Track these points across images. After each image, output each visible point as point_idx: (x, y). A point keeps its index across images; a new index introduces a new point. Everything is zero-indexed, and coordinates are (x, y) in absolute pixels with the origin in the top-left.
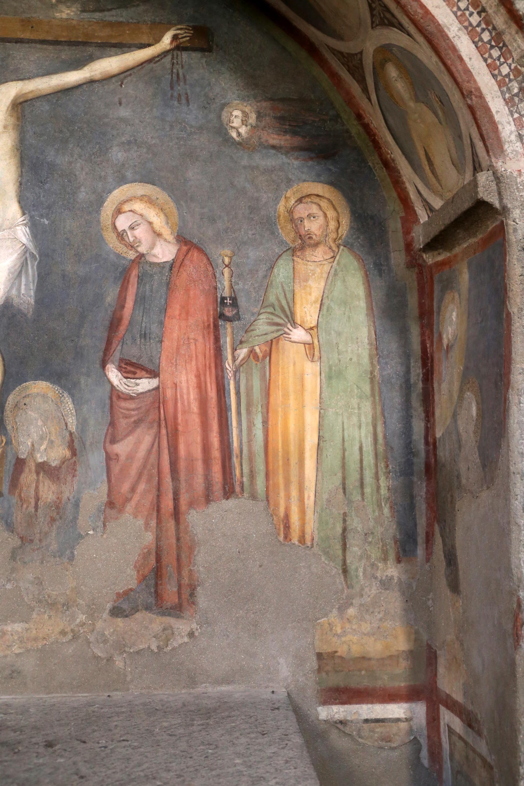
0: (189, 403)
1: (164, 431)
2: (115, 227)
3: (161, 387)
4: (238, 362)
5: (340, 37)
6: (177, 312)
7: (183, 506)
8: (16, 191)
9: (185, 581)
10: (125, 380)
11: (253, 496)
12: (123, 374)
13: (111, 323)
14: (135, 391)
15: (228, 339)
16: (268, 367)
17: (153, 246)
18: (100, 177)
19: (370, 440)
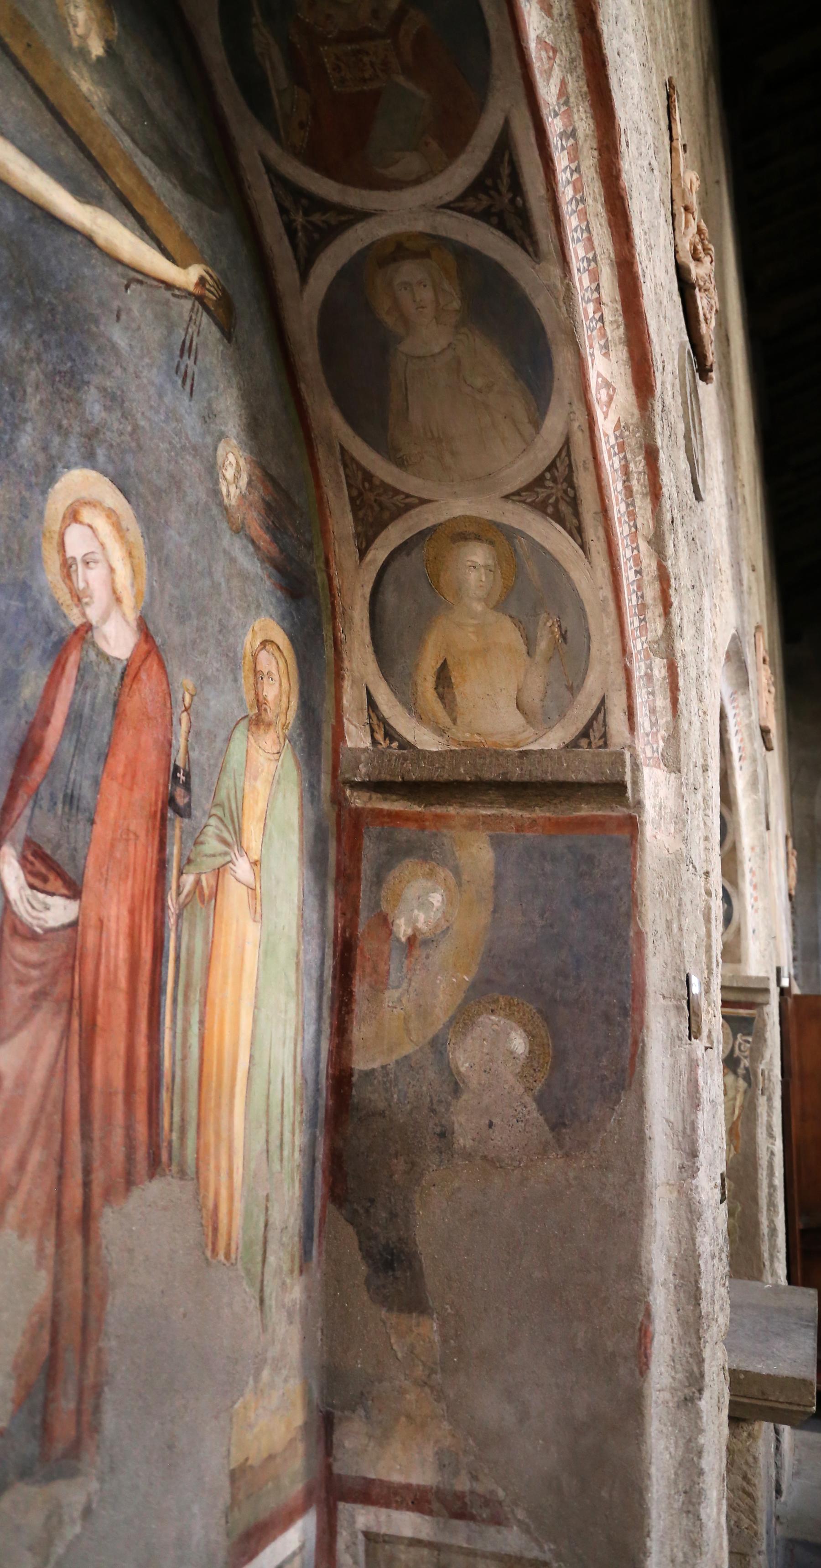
0: (116, 966)
1: (76, 1024)
2: (62, 545)
3: (80, 924)
4: (183, 896)
5: (401, 463)
6: (120, 770)
7: (97, 1202)
9: (90, 1380)
10: (29, 891)
11: (182, 1174)
12: (28, 875)
13: (23, 749)
14: (42, 923)
16: (212, 918)
17: (105, 617)
18: (60, 426)
19: (291, 1065)
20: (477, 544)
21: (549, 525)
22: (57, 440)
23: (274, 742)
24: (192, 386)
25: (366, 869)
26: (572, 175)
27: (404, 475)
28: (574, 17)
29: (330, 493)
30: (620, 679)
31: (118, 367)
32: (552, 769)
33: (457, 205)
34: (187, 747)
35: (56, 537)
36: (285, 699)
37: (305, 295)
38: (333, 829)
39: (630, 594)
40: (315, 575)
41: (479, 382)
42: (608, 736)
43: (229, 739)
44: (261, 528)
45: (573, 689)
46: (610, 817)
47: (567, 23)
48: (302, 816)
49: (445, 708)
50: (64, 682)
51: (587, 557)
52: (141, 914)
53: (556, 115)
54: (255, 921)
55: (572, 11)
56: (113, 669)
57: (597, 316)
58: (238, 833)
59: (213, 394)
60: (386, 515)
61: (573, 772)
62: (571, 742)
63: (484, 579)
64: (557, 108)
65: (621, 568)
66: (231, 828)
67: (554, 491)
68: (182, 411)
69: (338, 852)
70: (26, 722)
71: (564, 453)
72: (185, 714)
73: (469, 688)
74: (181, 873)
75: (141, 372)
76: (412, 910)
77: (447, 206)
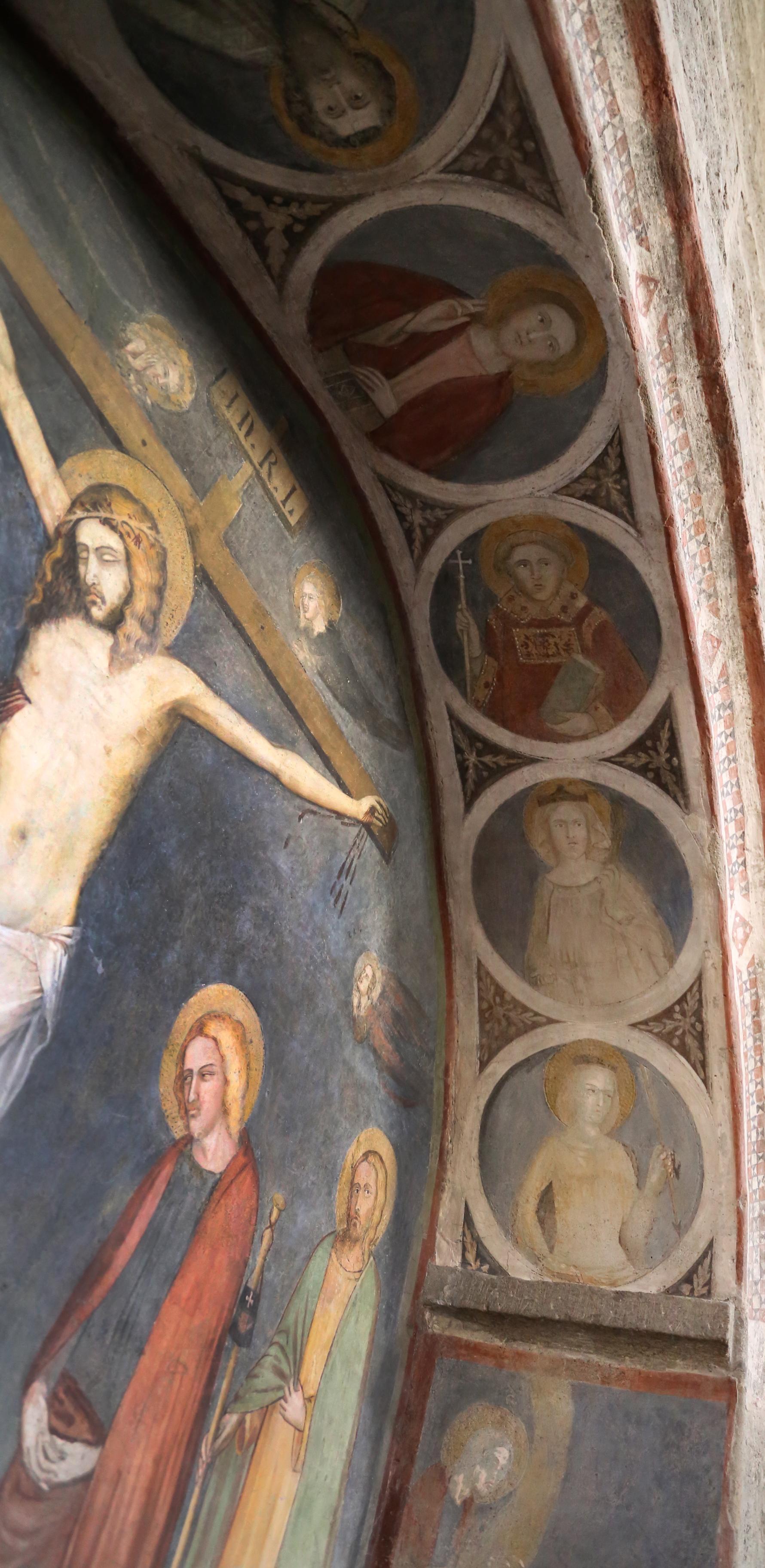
0: (121, 1532)
5: (534, 983)
6: (185, 1294)
8: (88, 866)
10: (47, 1437)
12: (53, 1416)
13: (88, 1270)
14: (51, 1476)
15: (224, 1385)
16: (246, 1467)
17: (207, 1131)
20: (600, 1068)
21: (673, 1056)
22: (201, 956)
23: (357, 1258)
24: (344, 904)
25: (432, 1407)
26: (726, 739)
27: (536, 993)
28: (738, 617)
29: (460, 1002)
30: (732, 1222)
31: (277, 888)
32: (649, 1316)
33: (617, 759)
34: (263, 1266)
35: (178, 1049)
36: (377, 1213)
37: (467, 823)
38: (403, 1358)
39: (750, 1130)
40: (432, 1084)
41: (620, 915)
42: (713, 1284)
43: (309, 1258)
44: (386, 1037)
45: (681, 1229)
46: (707, 1379)
47: (732, 622)
48: (372, 1342)
49: (543, 1234)
50: (150, 1197)
51: (708, 1092)
52: (167, 1463)
53: (716, 690)
54: (294, 1471)
55: (737, 614)
56: (204, 1182)
57: (740, 860)
58: (298, 1364)
59: (362, 911)
60: (513, 1030)
61: (671, 1323)
62: (672, 1286)
63: (601, 1104)
64: (717, 686)
65: (742, 1106)
66: (291, 1357)
67: (681, 1024)
68: (330, 927)
69: (405, 1385)
70: (99, 1241)
71: (695, 989)
72: (269, 1230)
73: (571, 1215)
74: (224, 1412)
75: (297, 893)
76: (474, 1466)
77: (609, 760)
